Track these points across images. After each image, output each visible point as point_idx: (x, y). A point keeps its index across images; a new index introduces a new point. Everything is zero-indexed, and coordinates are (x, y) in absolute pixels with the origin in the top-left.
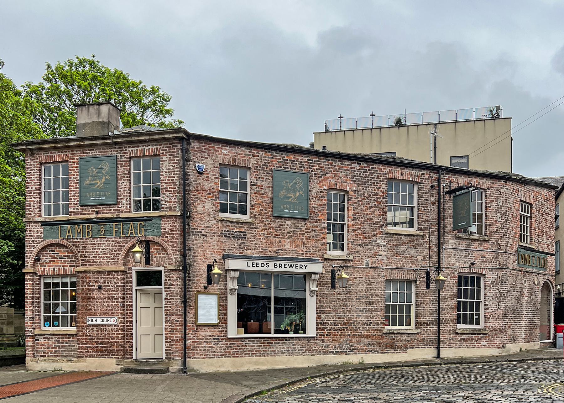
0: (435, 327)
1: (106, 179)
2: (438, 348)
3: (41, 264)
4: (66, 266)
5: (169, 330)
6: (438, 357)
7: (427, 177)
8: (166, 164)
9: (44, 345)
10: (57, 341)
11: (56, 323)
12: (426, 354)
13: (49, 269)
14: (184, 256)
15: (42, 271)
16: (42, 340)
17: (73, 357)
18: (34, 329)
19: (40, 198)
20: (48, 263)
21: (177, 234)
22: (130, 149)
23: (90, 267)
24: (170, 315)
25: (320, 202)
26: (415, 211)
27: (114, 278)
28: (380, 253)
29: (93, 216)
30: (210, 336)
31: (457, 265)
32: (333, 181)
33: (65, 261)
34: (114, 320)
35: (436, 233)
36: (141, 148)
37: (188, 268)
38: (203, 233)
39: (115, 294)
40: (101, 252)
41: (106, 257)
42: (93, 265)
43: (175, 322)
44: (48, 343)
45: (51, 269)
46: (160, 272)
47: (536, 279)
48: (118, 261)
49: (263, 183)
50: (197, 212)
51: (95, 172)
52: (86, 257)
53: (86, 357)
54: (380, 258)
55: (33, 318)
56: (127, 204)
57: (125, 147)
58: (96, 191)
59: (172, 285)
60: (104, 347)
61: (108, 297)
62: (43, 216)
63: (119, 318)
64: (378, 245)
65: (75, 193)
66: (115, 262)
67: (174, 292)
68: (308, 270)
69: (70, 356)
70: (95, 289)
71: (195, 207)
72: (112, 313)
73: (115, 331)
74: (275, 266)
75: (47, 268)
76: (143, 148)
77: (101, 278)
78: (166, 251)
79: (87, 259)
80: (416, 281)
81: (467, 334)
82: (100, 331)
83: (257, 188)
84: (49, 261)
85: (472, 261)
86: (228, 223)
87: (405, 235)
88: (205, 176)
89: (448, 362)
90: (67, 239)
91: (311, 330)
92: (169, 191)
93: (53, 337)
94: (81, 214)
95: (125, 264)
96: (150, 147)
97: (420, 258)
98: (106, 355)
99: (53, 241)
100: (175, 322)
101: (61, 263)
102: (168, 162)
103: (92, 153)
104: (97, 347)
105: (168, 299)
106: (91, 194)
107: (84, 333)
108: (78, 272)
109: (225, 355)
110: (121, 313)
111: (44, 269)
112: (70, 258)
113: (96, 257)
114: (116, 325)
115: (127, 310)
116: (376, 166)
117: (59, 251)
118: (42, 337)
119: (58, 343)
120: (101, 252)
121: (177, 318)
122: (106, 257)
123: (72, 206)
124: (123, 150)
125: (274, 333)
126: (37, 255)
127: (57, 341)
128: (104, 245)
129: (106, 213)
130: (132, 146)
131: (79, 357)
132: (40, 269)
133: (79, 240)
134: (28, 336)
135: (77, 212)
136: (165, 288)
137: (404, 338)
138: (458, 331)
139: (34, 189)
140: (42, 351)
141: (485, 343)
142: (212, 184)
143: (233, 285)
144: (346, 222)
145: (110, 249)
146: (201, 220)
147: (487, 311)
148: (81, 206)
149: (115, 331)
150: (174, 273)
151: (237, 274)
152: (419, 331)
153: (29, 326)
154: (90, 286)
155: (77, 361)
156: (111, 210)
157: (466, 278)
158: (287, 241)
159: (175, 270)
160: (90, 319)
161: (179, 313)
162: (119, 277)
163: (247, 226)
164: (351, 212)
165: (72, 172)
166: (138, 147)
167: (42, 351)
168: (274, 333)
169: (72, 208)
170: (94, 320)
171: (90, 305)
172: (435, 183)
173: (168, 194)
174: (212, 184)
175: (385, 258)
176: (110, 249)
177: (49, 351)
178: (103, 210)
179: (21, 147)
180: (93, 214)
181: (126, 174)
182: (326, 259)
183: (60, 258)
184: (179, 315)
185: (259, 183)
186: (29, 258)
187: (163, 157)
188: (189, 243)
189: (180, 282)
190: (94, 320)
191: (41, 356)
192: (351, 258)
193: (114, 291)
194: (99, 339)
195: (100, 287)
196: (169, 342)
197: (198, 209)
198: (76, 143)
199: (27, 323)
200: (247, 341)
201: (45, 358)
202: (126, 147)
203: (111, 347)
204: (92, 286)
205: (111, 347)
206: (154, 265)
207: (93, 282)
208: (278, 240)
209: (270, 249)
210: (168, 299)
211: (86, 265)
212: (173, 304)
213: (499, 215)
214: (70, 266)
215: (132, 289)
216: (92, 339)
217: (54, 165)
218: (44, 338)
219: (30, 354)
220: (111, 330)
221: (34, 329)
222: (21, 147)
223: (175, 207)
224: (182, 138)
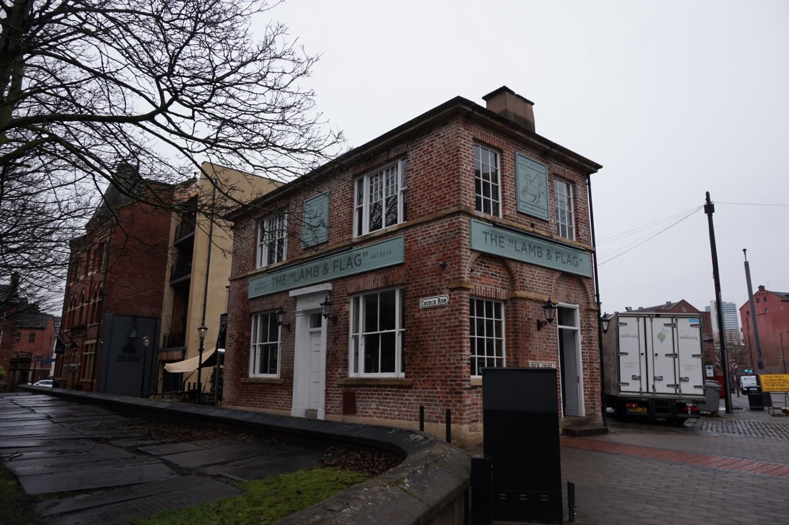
13: (481, 287)
84: (481, 275)
125: (394, 329)
168: (394, 329)
171: (530, 345)
183: (492, 275)
214: (502, 288)
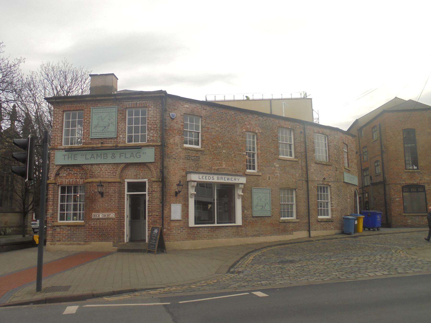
0: (307, 218)
2: (309, 231)
5: (150, 222)
6: (310, 237)
7: (298, 127)
8: (151, 112)
9: (60, 233)
12: (302, 234)
13: (66, 181)
14: (162, 172)
16: (58, 230)
17: (81, 241)
18: (53, 222)
19: (62, 133)
22: (127, 103)
24: (152, 212)
25: (241, 139)
26: (293, 147)
28: (276, 171)
29: (100, 145)
30: (178, 226)
31: (316, 180)
32: (248, 126)
34: (112, 215)
35: (305, 160)
36: (134, 102)
37: (165, 180)
38: (174, 157)
44: (63, 232)
47: (352, 188)
49: (209, 126)
50: (170, 143)
53: (91, 241)
54: (276, 174)
55: (53, 214)
56: (123, 138)
59: (154, 191)
61: (108, 199)
62: (63, 145)
63: (115, 214)
64: (275, 167)
67: (156, 196)
68: (237, 181)
69: (78, 241)
71: (169, 140)
72: (111, 210)
74: (218, 178)
76: (135, 102)
78: (149, 169)
80: (295, 189)
81: (324, 221)
83: (206, 129)
85: (324, 177)
86: (189, 151)
87: (289, 161)
88: (175, 121)
89: (318, 239)
91: (239, 221)
93: (67, 227)
94: (91, 144)
95: (121, 177)
96: (141, 102)
97: (297, 175)
102: (152, 111)
107: (90, 225)
108: (87, 183)
109: (187, 239)
111: (62, 181)
114: (113, 219)
115: (121, 209)
116: (271, 119)
118: (58, 228)
121: (157, 214)
126: (58, 171)
129: (108, 143)
131: (86, 242)
132: (59, 180)
137: (291, 225)
138: (319, 220)
139: (58, 127)
141: (332, 227)
142: (180, 126)
143: (192, 191)
144: (256, 152)
146: (173, 149)
147: (333, 208)
150: (155, 183)
151: (195, 184)
152: (298, 220)
154: (95, 192)
155: (84, 245)
157: (321, 187)
158: (224, 163)
159: (156, 181)
161: (159, 211)
163: (200, 153)
164: (259, 146)
166: (132, 101)
172: (302, 131)
173: (152, 131)
174: (180, 126)
175: (278, 174)
177: (63, 237)
179: (52, 101)
180: (99, 144)
181: (123, 119)
182: (246, 175)
184: (159, 212)
185: (207, 126)
188: (165, 163)
189: (159, 189)
191: (57, 241)
192: (260, 174)
193: (112, 196)
197: (171, 141)
198: (90, 99)
200: (201, 229)
201: (60, 242)
205: (109, 234)
208: (218, 162)
209: (214, 168)
213: (335, 151)
214: (81, 179)
215: (124, 194)
217: (73, 112)
221: (53, 222)
222: (52, 101)
223: (157, 140)
224: (163, 97)
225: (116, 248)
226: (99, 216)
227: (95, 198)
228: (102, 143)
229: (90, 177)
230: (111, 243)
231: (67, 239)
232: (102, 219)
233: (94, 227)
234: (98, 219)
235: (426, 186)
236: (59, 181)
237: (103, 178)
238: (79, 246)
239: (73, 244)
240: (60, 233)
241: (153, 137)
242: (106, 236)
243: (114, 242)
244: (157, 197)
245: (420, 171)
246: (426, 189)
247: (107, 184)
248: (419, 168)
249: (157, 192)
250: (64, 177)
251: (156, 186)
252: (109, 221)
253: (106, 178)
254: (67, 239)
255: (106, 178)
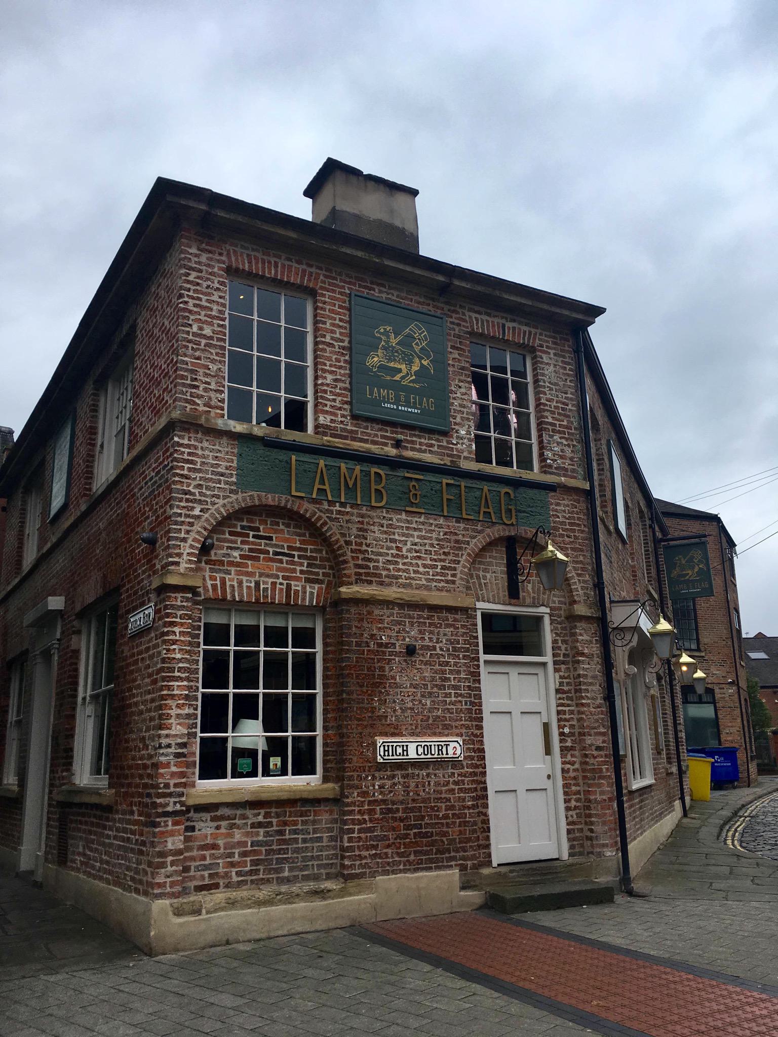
1: (422, 366)
3: (214, 562)
4: (297, 579)
5: (572, 774)
9: (215, 847)
10: (260, 825)
11: (275, 761)
13: (240, 583)
15: (214, 587)
16: (205, 828)
20: (238, 565)
21: (582, 532)
22: (474, 315)
23: (380, 588)
27: (448, 626)
33: (293, 563)
39: (451, 672)
40: (409, 551)
41: (425, 566)
42: (390, 584)
43: (595, 753)
44: (231, 835)
45: (248, 582)
46: (539, 619)
48: (453, 582)
51: (394, 341)
52: (370, 560)
53: (373, 875)
57: (461, 306)
58: (396, 386)
59: (583, 654)
60: (426, 835)
61: (433, 679)
65: (336, 380)
66: (447, 582)
67: (590, 674)
70: (397, 654)
72: (447, 727)
73: (456, 783)
75: (232, 579)
77: (412, 624)
79: (371, 565)
82: (413, 785)
90: (314, 501)
92: (559, 432)
93: (249, 813)
98: (431, 861)
99: (270, 499)
100: (595, 753)
101: (279, 569)
103: (380, 292)
104: (406, 836)
105: (564, 692)
106: (384, 392)
107: (364, 794)
110: (468, 727)
112: (306, 558)
113: (397, 563)
114: (455, 763)
117: (276, 532)
118: (207, 816)
119: (267, 834)
120: (409, 551)
122: (425, 566)
123: (327, 412)
124: (458, 313)
127: (260, 825)
128: (416, 534)
129: (420, 451)
130: (476, 308)
131: (347, 878)
133: (348, 509)
134: (167, 814)
135: (342, 430)
136: (555, 663)
139: (207, 331)
140: (206, 868)
145: (432, 545)
148: (354, 417)
149: (456, 783)
153: (173, 774)
154: (380, 645)
155: (343, 893)
156: (432, 445)
160: (387, 748)
161: (602, 730)
162: (459, 625)
165: (329, 322)
166: (489, 315)
167: (206, 868)
169: (329, 418)
170: (399, 750)
173: (557, 437)
176: (432, 545)
177: (232, 865)
178: (413, 442)
180: (386, 444)
186: (184, 540)
187: (544, 356)
190: (399, 750)
191: (199, 889)
193: (447, 664)
194: (412, 810)
195: (411, 651)
196: (576, 808)
199: (168, 765)
201: (219, 896)
202: (464, 307)
203: (445, 834)
204: (386, 645)
206: (528, 601)
207: (388, 632)
210: (564, 692)
211: (370, 582)
212: (588, 705)
214: (308, 580)
216: (389, 811)
218: (213, 819)
219: (173, 884)
220: (442, 780)
223: (573, 471)
225: (474, 896)
226: (405, 750)
227: (382, 669)
228: (398, 444)
229: (359, 580)
230: (454, 874)
231: (251, 873)
232: (415, 764)
233: (384, 801)
234: (400, 766)
235: (717, 691)
236: (209, 583)
237: (409, 586)
238: (319, 904)
239: (290, 898)
240: (215, 847)
241: (561, 457)
242: (432, 844)
243: (463, 868)
244: (594, 677)
245: (703, 654)
246: (717, 696)
247: (425, 614)
248: (702, 649)
249: (590, 656)
250: (231, 564)
251: (585, 637)
252: (440, 773)
253: (419, 587)
254: (251, 873)
255: (419, 587)
